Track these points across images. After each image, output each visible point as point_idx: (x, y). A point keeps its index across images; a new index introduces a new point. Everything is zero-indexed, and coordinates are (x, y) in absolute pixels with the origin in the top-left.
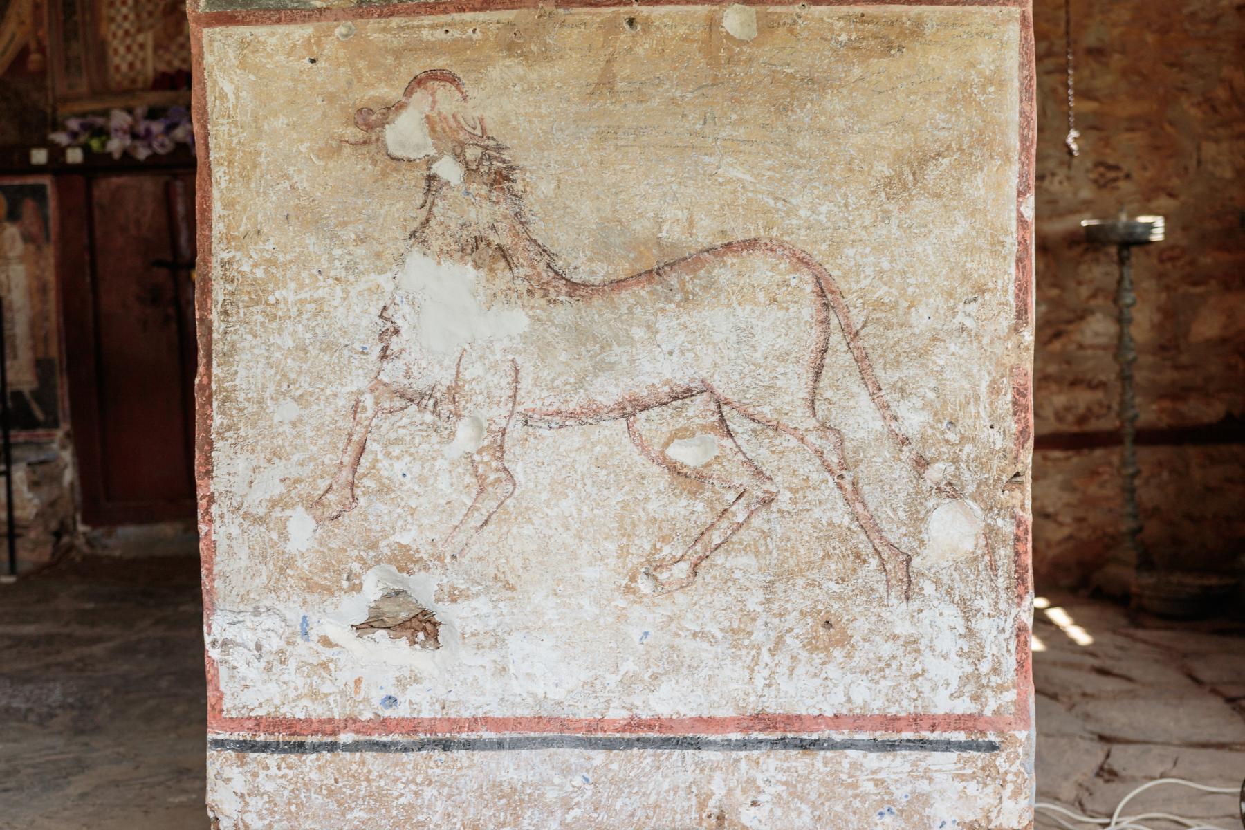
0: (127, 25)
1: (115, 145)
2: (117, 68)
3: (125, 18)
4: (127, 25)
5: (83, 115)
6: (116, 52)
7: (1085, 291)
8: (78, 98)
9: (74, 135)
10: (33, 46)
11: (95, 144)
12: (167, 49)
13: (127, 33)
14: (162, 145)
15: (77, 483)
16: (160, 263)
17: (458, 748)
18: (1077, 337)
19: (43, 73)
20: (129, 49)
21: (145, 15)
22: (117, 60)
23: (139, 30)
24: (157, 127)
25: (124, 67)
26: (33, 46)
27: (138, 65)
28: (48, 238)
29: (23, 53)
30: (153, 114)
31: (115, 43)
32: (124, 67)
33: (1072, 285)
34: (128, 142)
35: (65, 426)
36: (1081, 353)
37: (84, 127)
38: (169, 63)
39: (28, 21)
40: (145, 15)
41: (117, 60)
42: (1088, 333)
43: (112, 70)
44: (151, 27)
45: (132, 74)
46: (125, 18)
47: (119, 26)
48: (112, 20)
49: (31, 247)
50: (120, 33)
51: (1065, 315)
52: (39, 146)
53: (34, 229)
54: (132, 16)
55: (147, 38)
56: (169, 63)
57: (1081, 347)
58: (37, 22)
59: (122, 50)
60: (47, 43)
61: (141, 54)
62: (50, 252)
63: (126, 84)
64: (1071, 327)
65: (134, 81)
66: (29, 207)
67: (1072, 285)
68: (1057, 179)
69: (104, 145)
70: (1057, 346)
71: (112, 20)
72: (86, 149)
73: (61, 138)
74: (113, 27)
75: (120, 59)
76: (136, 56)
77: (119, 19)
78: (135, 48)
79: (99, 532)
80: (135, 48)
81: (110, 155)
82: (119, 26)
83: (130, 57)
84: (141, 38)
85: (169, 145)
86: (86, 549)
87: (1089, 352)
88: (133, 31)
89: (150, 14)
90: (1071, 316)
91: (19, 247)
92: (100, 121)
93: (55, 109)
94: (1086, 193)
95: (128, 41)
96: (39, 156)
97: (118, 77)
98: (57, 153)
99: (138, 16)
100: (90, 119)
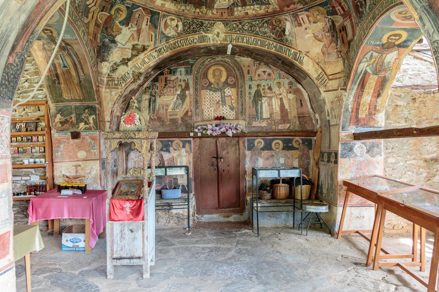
0: (208, 106)
1: (209, 132)
2: (206, 115)
3: (208, 104)
4: (208, 106)
5: (201, 125)
6: (205, 112)
7: (435, 170)
8: (199, 122)
9: (199, 130)
10: (189, 110)
11: (204, 132)
12: (217, 111)
13: (208, 108)
14: (218, 132)
15: (195, 205)
16: (214, 157)
17: (75, 187)
18: (433, 180)
19: (191, 116)
20: (208, 111)
21: (212, 104)
22: (206, 113)
23: (211, 107)
24: (217, 128)
25: (207, 115)
26: (189, 110)
27: (210, 115)
28: (191, 152)
29: (187, 112)
30: (216, 126)
31: (205, 110)
32: (207, 115)
33: (432, 169)
34: (211, 131)
35: (193, 193)
36: (434, 184)
37: (201, 128)
38: (217, 114)
39: (189, 105)
40: (212, 104)
41: (206, 113)
42: (435, 180)
43: (204, 116)
44: (213, 107)
45: (209, 116)
46: (208, 104)
47: (206, 106)
48: (205, 105)
49: (187, 154)
50: (207, 108)
51: (430, 175)
52: (192, 132)
53: (188, 150)
54: (209, 104)
55: (212, 109)
56: (217, 114)
57: (434, 182)
58: (190, 105)
59: (207, 111)
60: (192, 110)
61: (211, 112)
62: (191, 155)
63: (207, 119)
64: (432, 178)
65: (209, 118)
66: (187, 145)
67: (432, 169)
68: (429, 146)
69: (206, 132)
70: (429, 182)
71: (205, 105)
72: (202, 133)
73: (196, 130)
74: (205, 106)
75: (206, 113)
76: (210, 113)
77: (206, 105)
78: (210, 111)
79: (200, 216)
80: (210, 111)
81: (208, 134)
82: (206, 106)
83: (208, 113)
84: (211, 109)
85: (220, 133)
86: (197, 220)
87: (436, 184)
88: (209, 107)
89: (213, 104)
90: (432, 176)
91: (185, 154)
92: (205, 127)
93: (194, 124)
94: (435, 149)
95: (208, 109)
96: (192, 134)
97: (206, 117)
98: (196, 133)
99: (210, 104)
100: (203, 126)
